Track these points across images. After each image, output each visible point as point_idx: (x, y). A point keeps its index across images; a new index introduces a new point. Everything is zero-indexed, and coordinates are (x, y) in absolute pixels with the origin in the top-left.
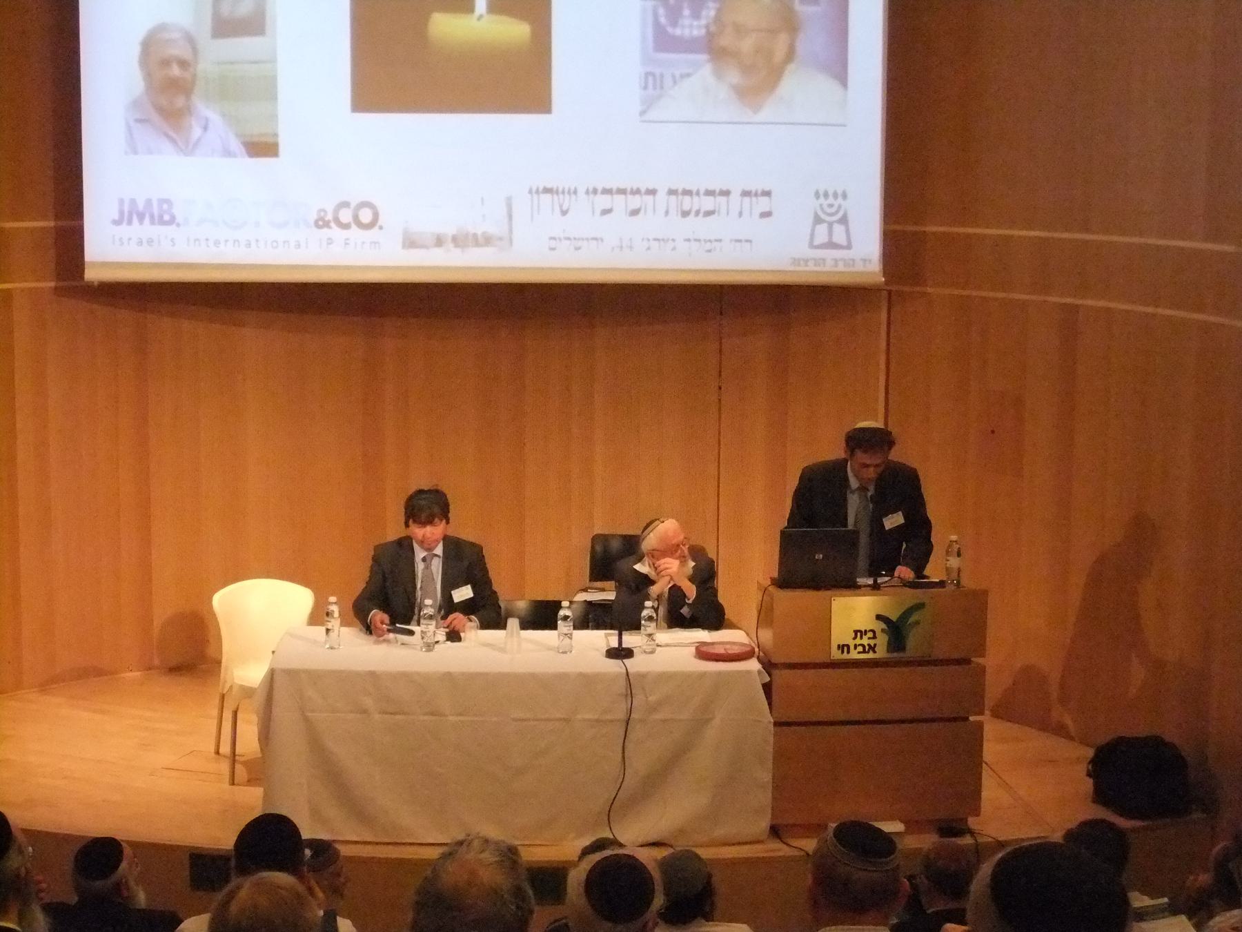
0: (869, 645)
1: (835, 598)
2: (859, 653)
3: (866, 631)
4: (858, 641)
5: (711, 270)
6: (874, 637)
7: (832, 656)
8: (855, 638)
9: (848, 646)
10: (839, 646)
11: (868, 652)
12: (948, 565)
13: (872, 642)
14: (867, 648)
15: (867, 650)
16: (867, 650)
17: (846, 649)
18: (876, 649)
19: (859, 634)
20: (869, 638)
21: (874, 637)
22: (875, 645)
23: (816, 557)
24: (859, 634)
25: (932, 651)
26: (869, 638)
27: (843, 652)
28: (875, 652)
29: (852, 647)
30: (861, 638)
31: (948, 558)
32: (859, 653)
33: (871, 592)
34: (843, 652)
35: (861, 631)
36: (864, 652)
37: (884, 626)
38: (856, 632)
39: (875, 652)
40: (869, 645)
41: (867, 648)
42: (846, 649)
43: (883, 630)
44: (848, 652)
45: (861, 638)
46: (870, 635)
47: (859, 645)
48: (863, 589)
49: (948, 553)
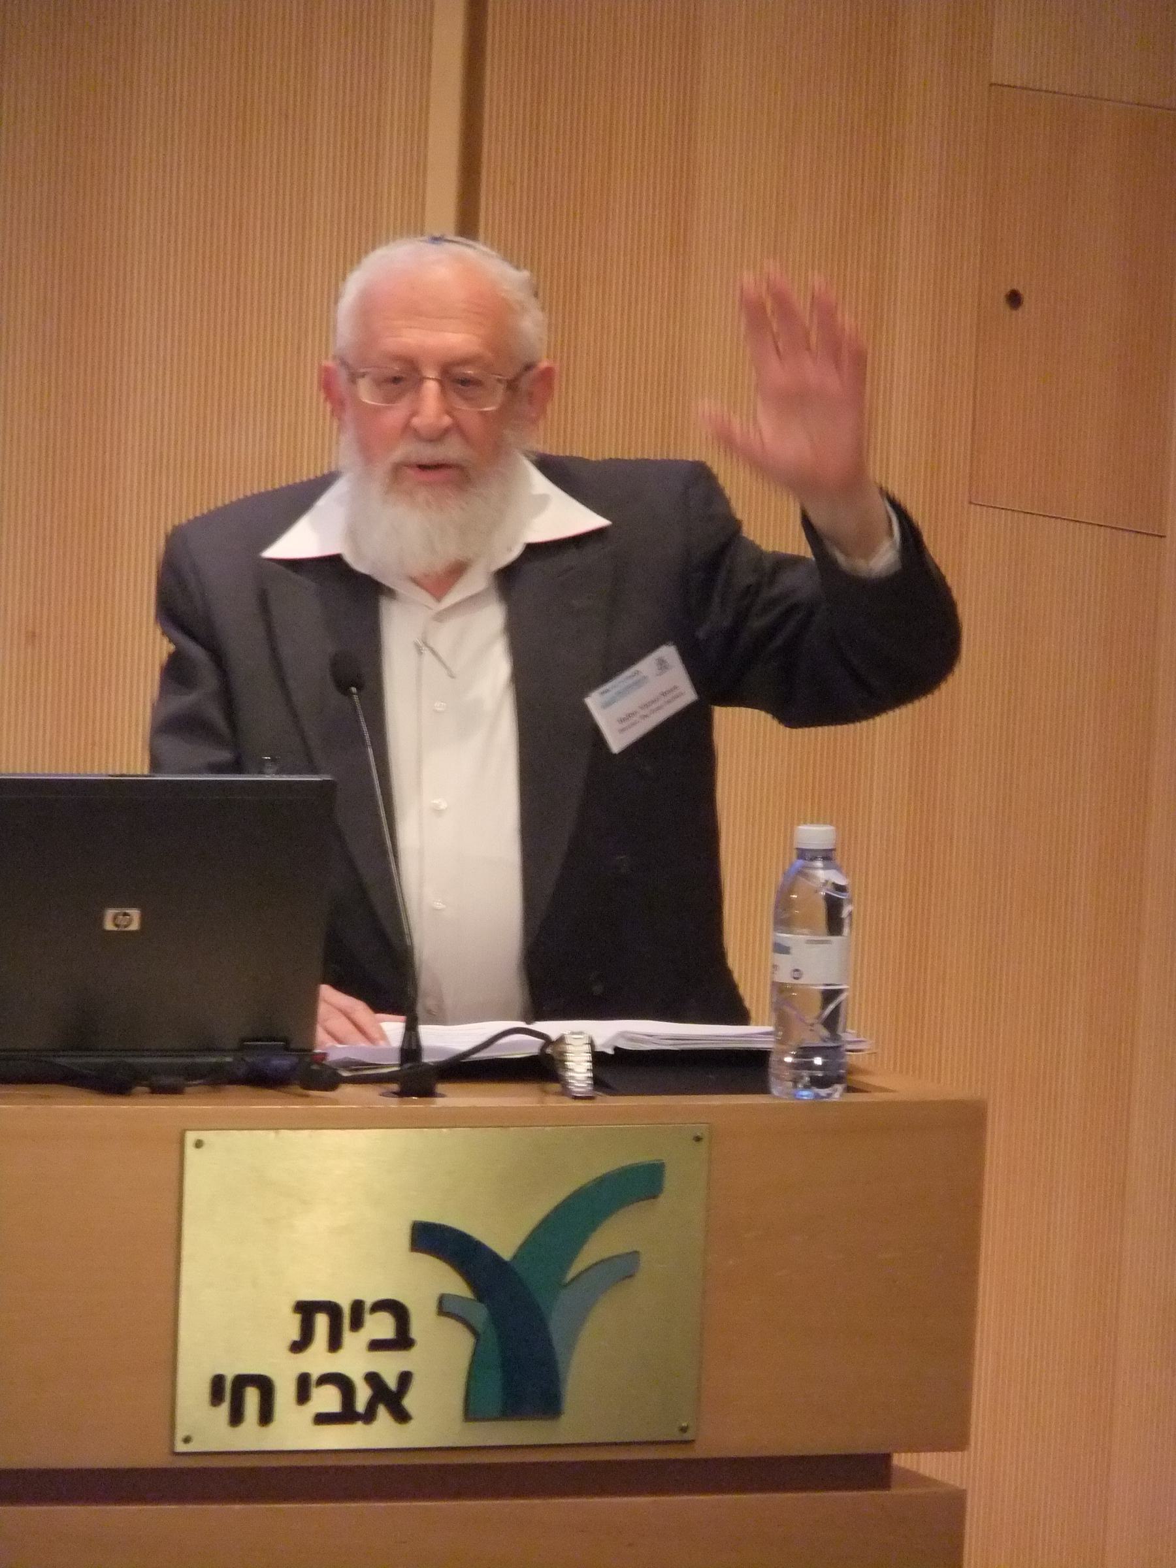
0: (373, 1379)
1: (204, 1135)
2: (322, 1419)
3: (357, 1306)
4: (318, 1361)
5: (596, 1264)
6: (402, 1341)
7: (180, 1434)
8: (299, 1346)
9: (265, 1386)
10: (217, 1383)
11: (369, 1416)
12: (784, 977)
13: (389, 1366)
14: (363, 1394)
15: (360, 1406)
16: (360, 1406)
17: (252, 1397)
18: (408, 1402)
19: (322, 1322)
20: (376, 1345)
21: (402, 1341)
22: (405, 1379)
23: (109, 926)
24: (322, 1322)
25: (782, 1080)
26: (376, 1345)
27: (236, 1417)
28: (402, 1416)
29: (285, 1393)
30: (335, 1343)
31: (785, 937)
32: (322, 1419)
33: (394, 1103)
34: (236, 1417)
35: (333, 1310)
36: (347, 1415)
37: (455, 1285)
38: (306, 1310)
39: (402, 1416)
40: (373, 1379)
41: (363, 1394)
42: (252, 1397)
43: (445, 1307)
44: (266, 1416)
45: (335, 1343)
46: (381, 1326)
47: (326, 1379)
48: (347, 1090)
49: (784, 919)
